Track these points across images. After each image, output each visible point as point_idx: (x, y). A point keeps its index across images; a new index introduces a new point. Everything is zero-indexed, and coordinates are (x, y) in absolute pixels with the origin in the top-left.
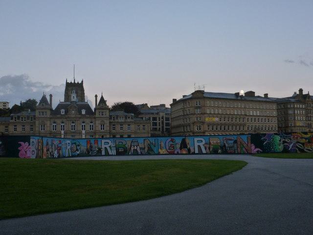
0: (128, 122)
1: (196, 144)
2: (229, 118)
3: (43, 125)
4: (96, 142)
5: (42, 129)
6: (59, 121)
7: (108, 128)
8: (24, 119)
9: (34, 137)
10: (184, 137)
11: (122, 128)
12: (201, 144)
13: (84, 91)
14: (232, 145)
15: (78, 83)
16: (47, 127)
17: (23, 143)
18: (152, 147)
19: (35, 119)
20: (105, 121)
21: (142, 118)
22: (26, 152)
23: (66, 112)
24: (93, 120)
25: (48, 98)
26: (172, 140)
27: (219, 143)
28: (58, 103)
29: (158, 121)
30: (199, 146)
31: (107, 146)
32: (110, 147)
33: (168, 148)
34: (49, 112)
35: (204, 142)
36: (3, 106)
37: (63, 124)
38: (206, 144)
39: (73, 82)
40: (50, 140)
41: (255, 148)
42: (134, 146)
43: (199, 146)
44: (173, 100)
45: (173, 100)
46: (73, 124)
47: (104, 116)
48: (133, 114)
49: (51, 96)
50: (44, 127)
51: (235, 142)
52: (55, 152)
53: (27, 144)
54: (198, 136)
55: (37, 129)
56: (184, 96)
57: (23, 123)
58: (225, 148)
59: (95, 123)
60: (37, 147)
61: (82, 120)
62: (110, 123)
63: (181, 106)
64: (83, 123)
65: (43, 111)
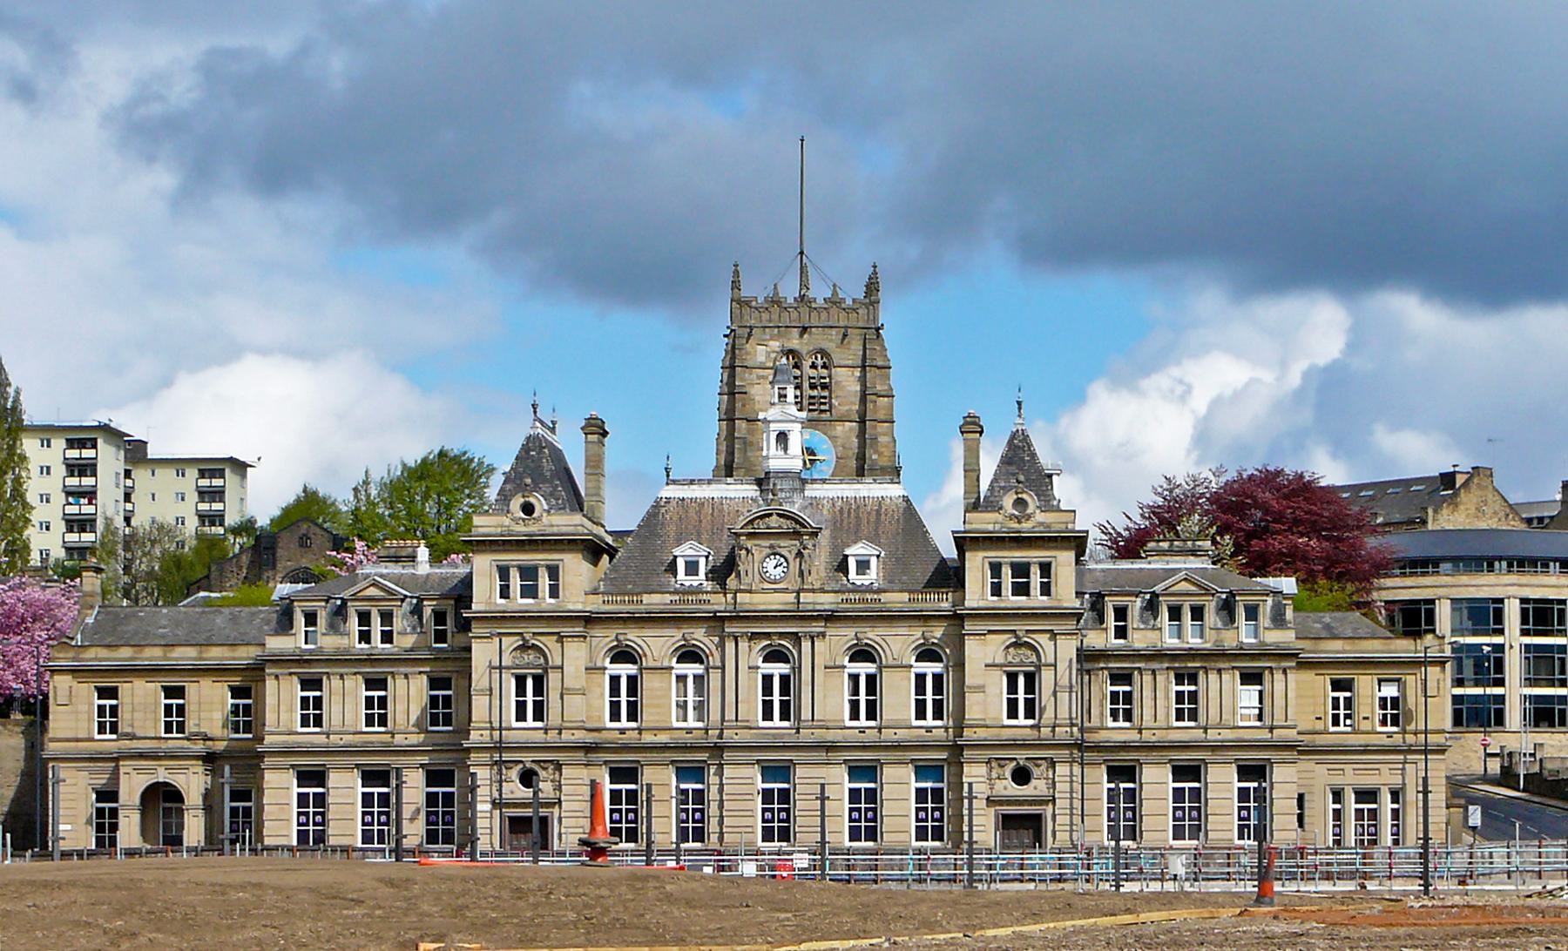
0: (1240, 654)
2: (387, 617)
3: (535, 683)
5: (521, 707)
6: (657, 645)
8: (377, 628)
11: (1188, 707)
15: (834, 302)
19: (464, 626)
20: (550, 643)
21: (1414, 619)
23: (723, 571)
25: (572, 447)
36: (203, 494)
46: (778, 669)
47: (1037, 599)
48: (1288, 584)
49: (596, 429)
50: (539, 690)
57: (371, 660)
59: (960, 665)
65: (1019, 555)
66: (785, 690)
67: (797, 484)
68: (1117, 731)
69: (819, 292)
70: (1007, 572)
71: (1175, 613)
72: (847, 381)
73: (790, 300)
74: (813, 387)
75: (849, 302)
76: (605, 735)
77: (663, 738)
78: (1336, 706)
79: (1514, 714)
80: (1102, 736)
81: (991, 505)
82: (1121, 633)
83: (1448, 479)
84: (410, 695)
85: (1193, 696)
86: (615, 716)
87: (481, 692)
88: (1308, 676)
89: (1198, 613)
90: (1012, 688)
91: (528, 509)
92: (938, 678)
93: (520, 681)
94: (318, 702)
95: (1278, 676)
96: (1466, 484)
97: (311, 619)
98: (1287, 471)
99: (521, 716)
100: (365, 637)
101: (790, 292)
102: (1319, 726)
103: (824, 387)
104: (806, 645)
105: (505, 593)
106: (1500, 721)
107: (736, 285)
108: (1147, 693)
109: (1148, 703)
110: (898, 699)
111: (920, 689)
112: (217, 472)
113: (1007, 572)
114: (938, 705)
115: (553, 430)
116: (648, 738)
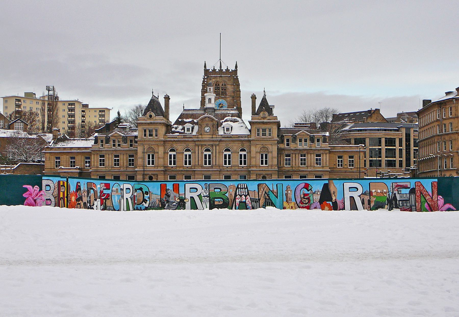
1: (348, 194)
3: (152, 157)
4: (176, 188)
5: (149, 161)
7: (275, 162)
8: (117, 144)
9: (51, 178)
10: (327, 182)
11: (303, 162)
12: (356, 195)
13: (238, 85)
14: (406, 197)
15: (227, 70)
16: (159, 158)
17: (31, 187)
18: (272, 197)
22: (35, 201)
24: (246, 145)
26: (307, 187)
27: (386, 193)
28: (181, 111)
29: (397, 147)
30: (352, 198)
31: (195, 195)
32: (199, 196)
33: (298, 200)
34: (162, 130)
35: (360, 192)
36: (100, 116)
37: (243, 153)
38: (364, 194)
39: (217, 69)
40: (83, 183)
41: (445, 204)
42: (241, 196)
43: (352, 198)
44: (424, 101)
45: (424, 101)
46: (208, 153)
49: (167, 98)
50: (266, 158)
51: (413, 191)
52: (95, 203)
53: (37, 188)
54: (351, 179)
55: (140, 161)
56: (448, 93)
58: (396, 203)
60: (56, 193)
61: (223, 146)
62: (280, 151)
63: (434, 115)
64: (227, 150)
65: (264, 126)
66: (209, 158)
67: (213, 110)
68: (287, 167)
69: (224, 68)
70: (261, 130)
71: (300, 141)
72: (230, 88)
73: (217, 70)
74: (222, 90)
75: (231, 71)
76: (168, 168)
77: (181, 169)
78: (339, 162)
79: (383, 164)
80: (284, 168)
81: (257, 114)
82: (288, 145)
83: (370, 111)
84: (124, 160)
85: (305, 159)
86: (171, 164)
87: (275, 157)
88: (332, 155)
89: (306, 141)
90: (262, 158)
91: (151, 116)
92: (245, 155)
93: (149, 156)
94: (104, 160)
95: (325, 155)
96: (374, 113)
97: (102, 141)
98: (331, 108)
99: (149, 164)
100: (114, 145)
101: (217, 69)
102: (335, 166)
103: (225, 90)
104: (214, 147)
105: (145, 135)
106: (380, 165)
107: (205, 66)
108: (294, 159)
109: (294, 161)
110: (235, 160)
111: (241, 158)
112: (103, 112)
113: (261, 130)
114: (245, 161)
115: (158, 98)
116: (178, 169)
